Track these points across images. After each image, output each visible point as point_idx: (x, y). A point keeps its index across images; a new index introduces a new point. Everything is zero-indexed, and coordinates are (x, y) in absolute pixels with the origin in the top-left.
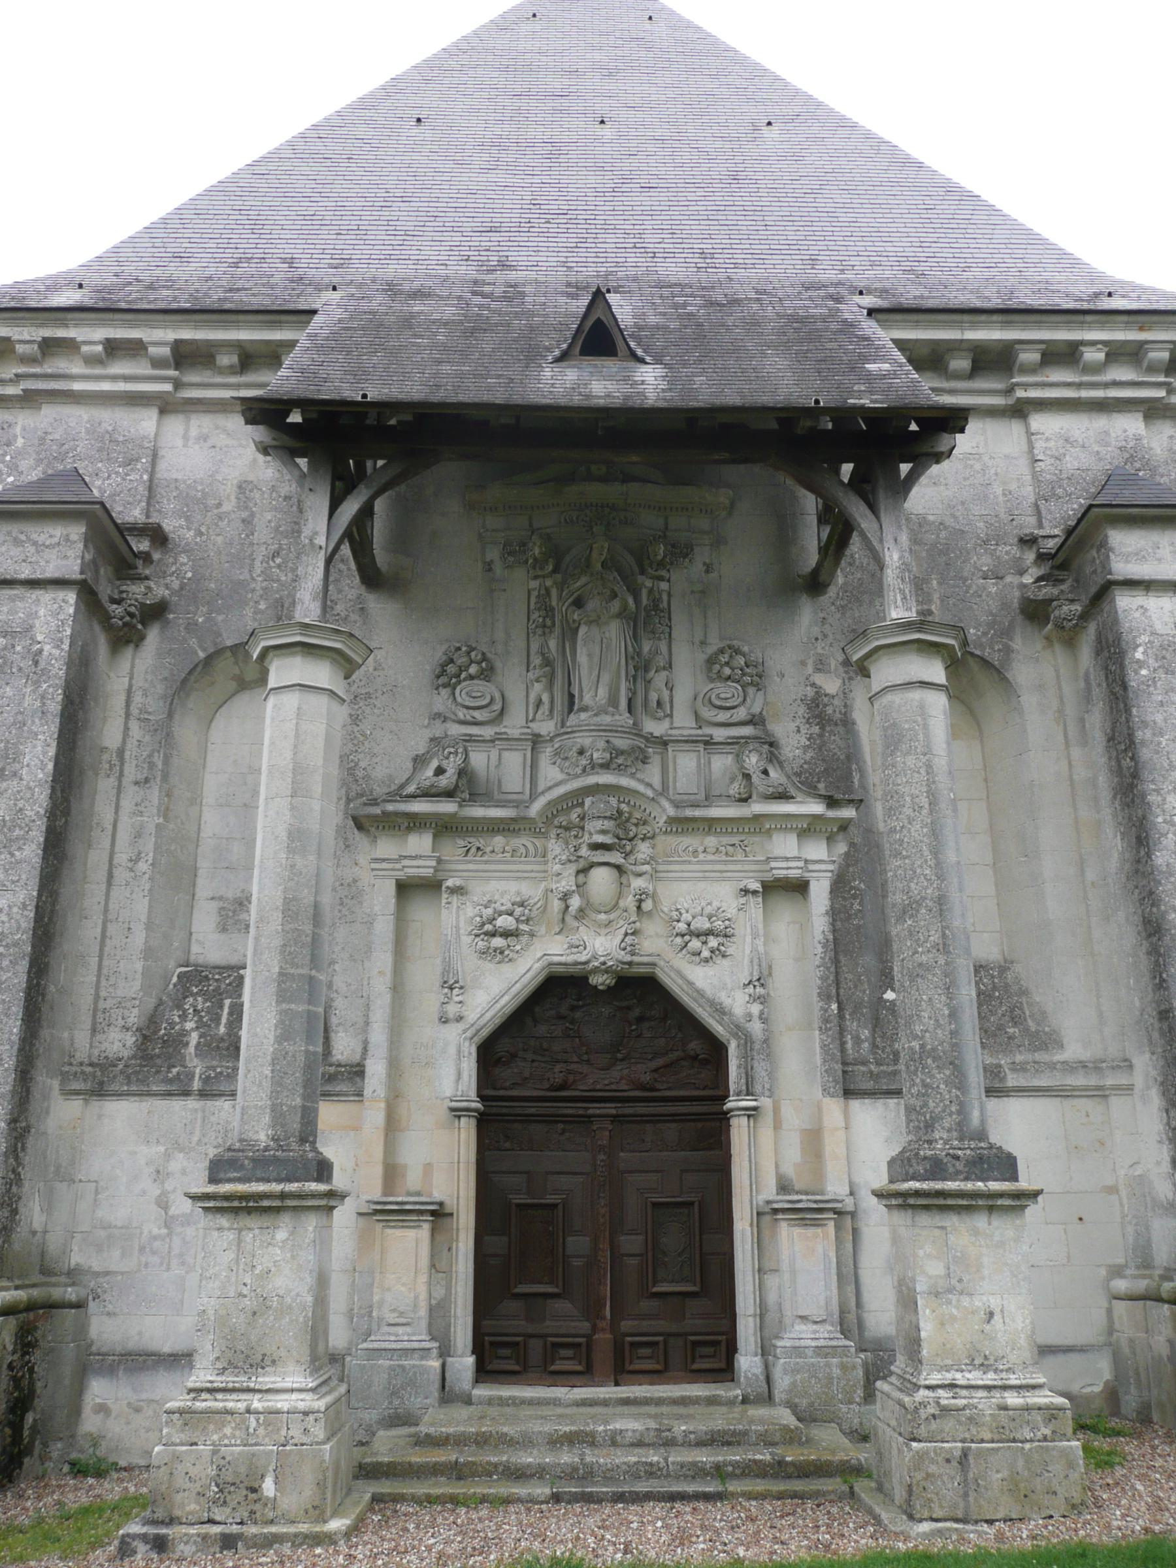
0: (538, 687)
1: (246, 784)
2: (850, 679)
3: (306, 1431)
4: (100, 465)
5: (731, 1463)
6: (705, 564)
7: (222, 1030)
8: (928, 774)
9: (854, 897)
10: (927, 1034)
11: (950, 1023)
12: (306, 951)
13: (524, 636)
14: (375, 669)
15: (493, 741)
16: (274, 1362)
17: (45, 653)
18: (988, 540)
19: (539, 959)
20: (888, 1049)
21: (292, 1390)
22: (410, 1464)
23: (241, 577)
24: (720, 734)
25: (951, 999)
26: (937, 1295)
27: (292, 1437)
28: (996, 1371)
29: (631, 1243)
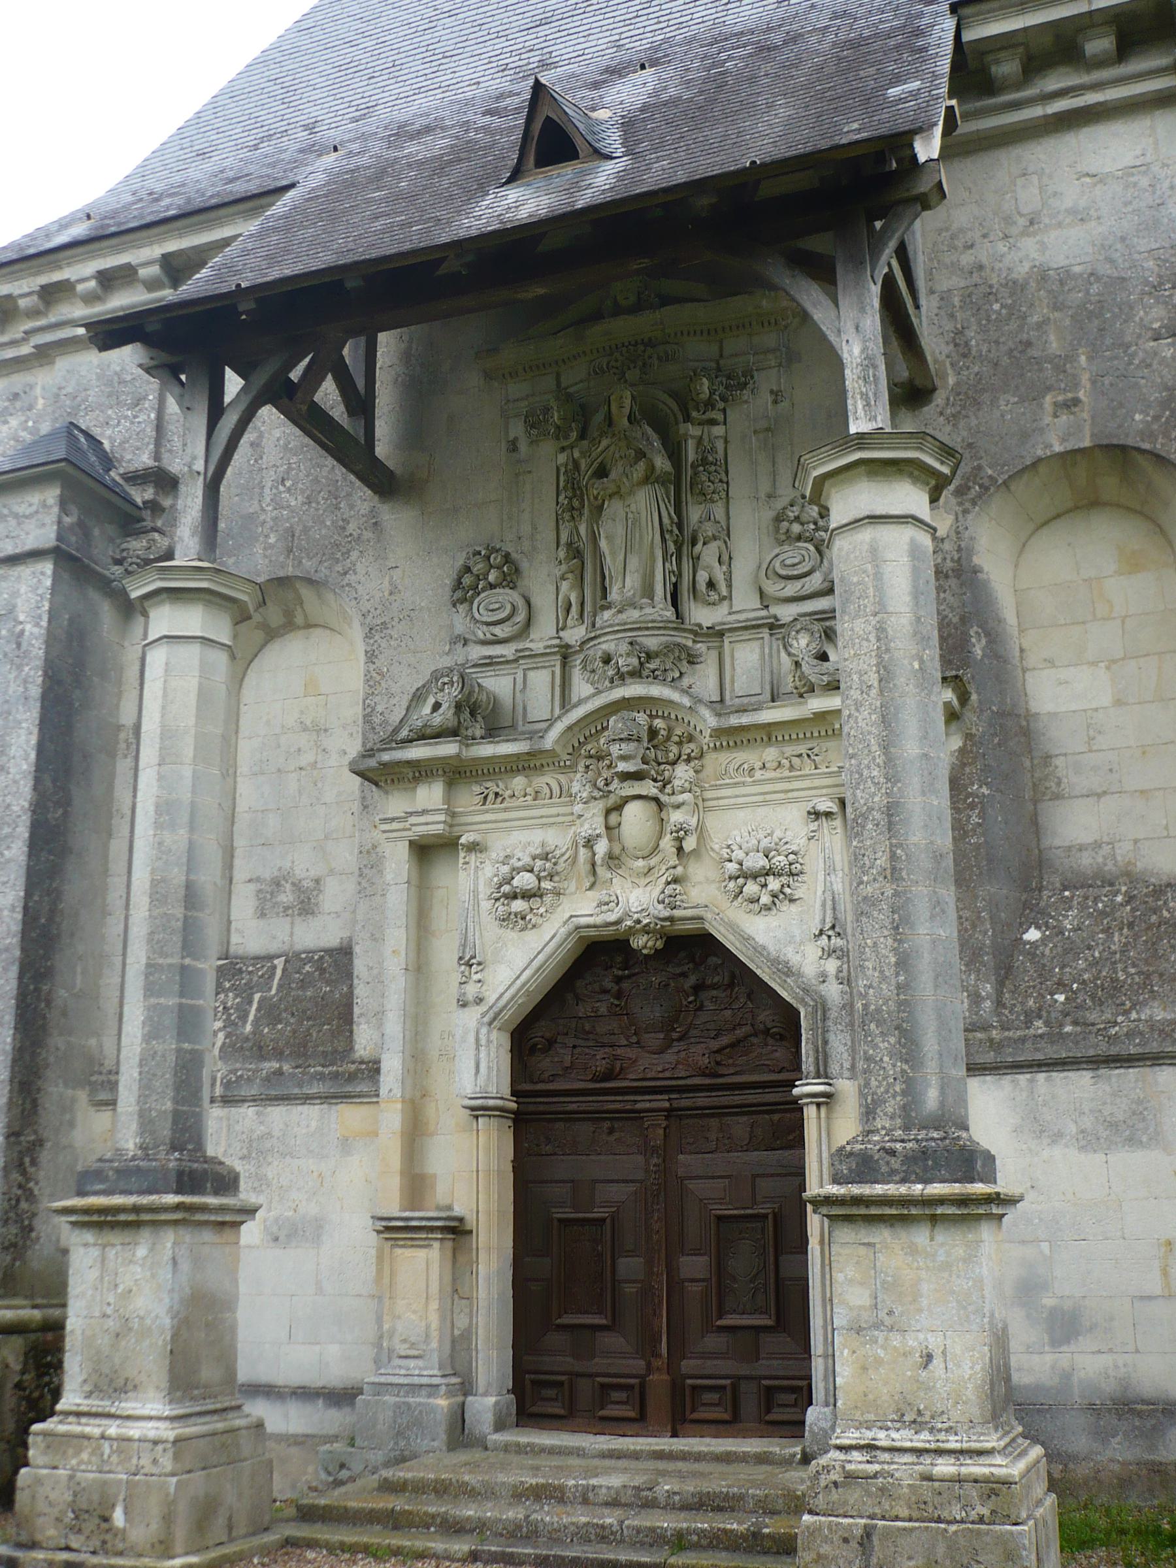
0: (565, 586)
1: (279, 746)
2: (966, 512)
3: (155, 1462)
4: (110, 412)
5: (696, 1532)
6: (772, 392)
7: (248, 1028)
8: (879, 639)
9: (972, 806)
10: (871, 991)
11: (897, 974)
12: (177, 939)
13: (553, 524)
14: (391, 594)
15: (516, 661)
16: (135, 1387)
17: (27, 633)
18: (1161, 284)
19: (565, 923)
20: (1018, 1009)
21: (150, 1418)
22: (346, 1508)
23: (251, 510)
24: (786, 613)
25: (900, 942)
26: (859, 1331)
27: (143, 1467)
28: (932, 1430)
29: (694, 1266)
